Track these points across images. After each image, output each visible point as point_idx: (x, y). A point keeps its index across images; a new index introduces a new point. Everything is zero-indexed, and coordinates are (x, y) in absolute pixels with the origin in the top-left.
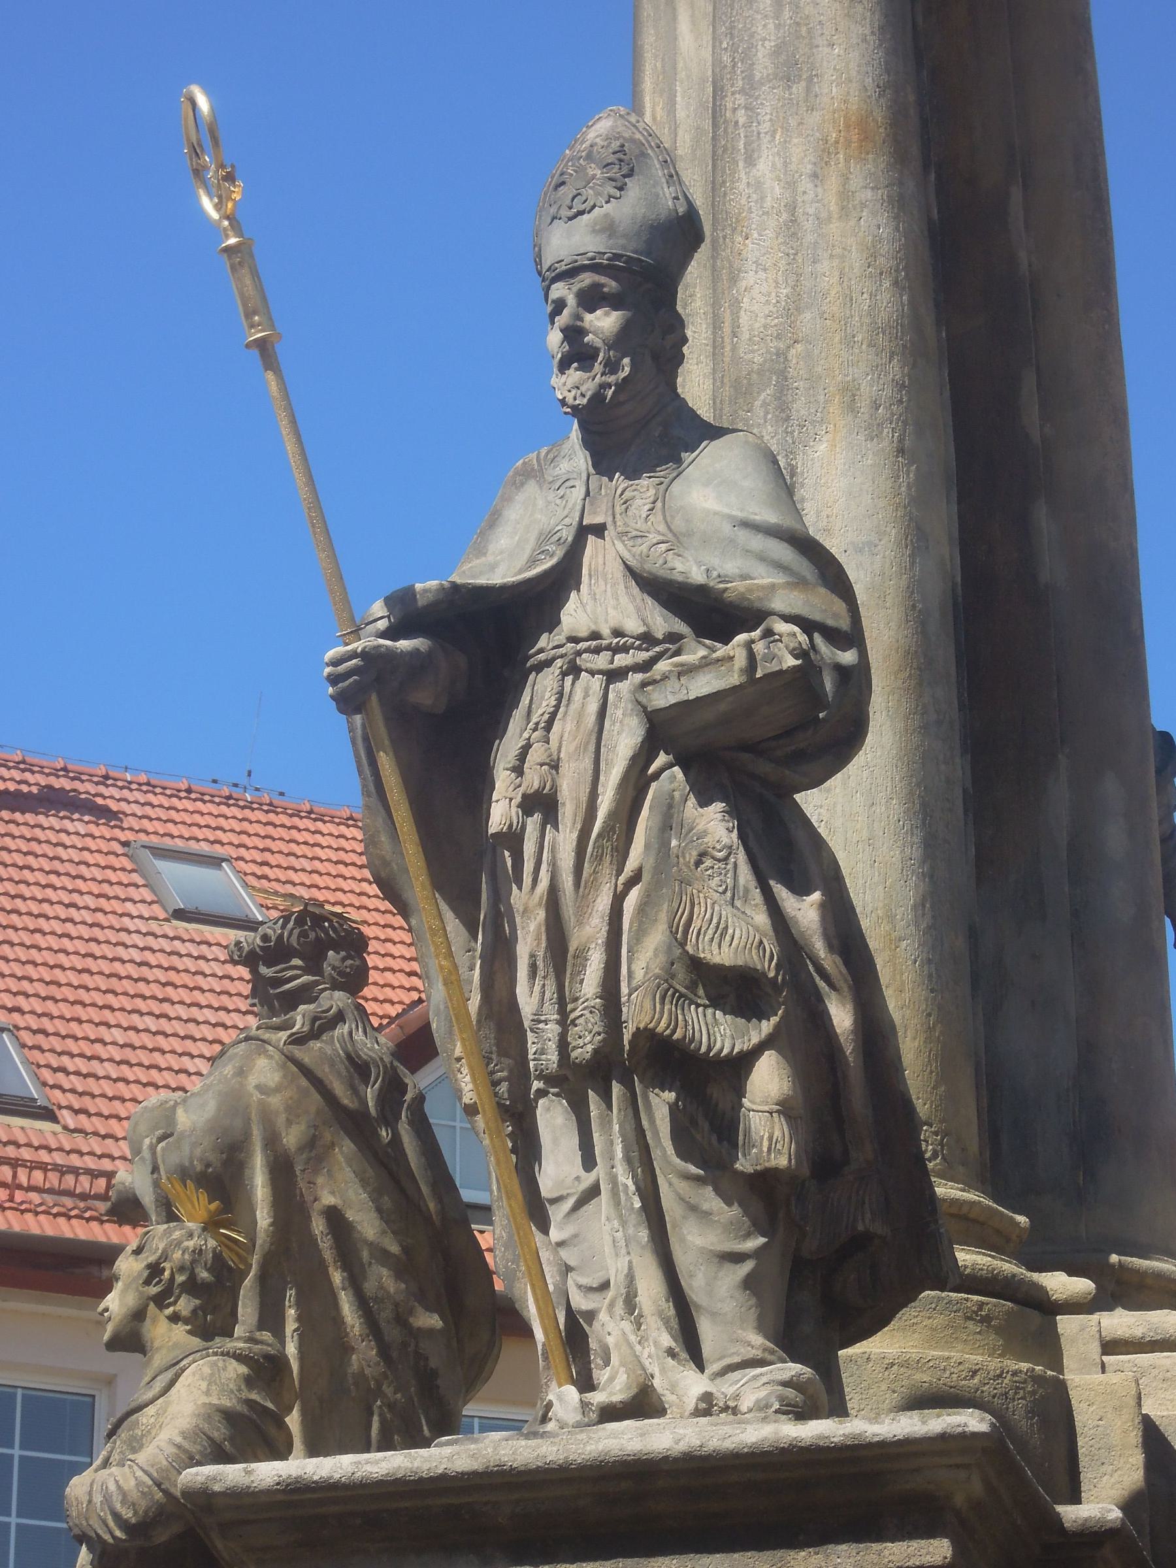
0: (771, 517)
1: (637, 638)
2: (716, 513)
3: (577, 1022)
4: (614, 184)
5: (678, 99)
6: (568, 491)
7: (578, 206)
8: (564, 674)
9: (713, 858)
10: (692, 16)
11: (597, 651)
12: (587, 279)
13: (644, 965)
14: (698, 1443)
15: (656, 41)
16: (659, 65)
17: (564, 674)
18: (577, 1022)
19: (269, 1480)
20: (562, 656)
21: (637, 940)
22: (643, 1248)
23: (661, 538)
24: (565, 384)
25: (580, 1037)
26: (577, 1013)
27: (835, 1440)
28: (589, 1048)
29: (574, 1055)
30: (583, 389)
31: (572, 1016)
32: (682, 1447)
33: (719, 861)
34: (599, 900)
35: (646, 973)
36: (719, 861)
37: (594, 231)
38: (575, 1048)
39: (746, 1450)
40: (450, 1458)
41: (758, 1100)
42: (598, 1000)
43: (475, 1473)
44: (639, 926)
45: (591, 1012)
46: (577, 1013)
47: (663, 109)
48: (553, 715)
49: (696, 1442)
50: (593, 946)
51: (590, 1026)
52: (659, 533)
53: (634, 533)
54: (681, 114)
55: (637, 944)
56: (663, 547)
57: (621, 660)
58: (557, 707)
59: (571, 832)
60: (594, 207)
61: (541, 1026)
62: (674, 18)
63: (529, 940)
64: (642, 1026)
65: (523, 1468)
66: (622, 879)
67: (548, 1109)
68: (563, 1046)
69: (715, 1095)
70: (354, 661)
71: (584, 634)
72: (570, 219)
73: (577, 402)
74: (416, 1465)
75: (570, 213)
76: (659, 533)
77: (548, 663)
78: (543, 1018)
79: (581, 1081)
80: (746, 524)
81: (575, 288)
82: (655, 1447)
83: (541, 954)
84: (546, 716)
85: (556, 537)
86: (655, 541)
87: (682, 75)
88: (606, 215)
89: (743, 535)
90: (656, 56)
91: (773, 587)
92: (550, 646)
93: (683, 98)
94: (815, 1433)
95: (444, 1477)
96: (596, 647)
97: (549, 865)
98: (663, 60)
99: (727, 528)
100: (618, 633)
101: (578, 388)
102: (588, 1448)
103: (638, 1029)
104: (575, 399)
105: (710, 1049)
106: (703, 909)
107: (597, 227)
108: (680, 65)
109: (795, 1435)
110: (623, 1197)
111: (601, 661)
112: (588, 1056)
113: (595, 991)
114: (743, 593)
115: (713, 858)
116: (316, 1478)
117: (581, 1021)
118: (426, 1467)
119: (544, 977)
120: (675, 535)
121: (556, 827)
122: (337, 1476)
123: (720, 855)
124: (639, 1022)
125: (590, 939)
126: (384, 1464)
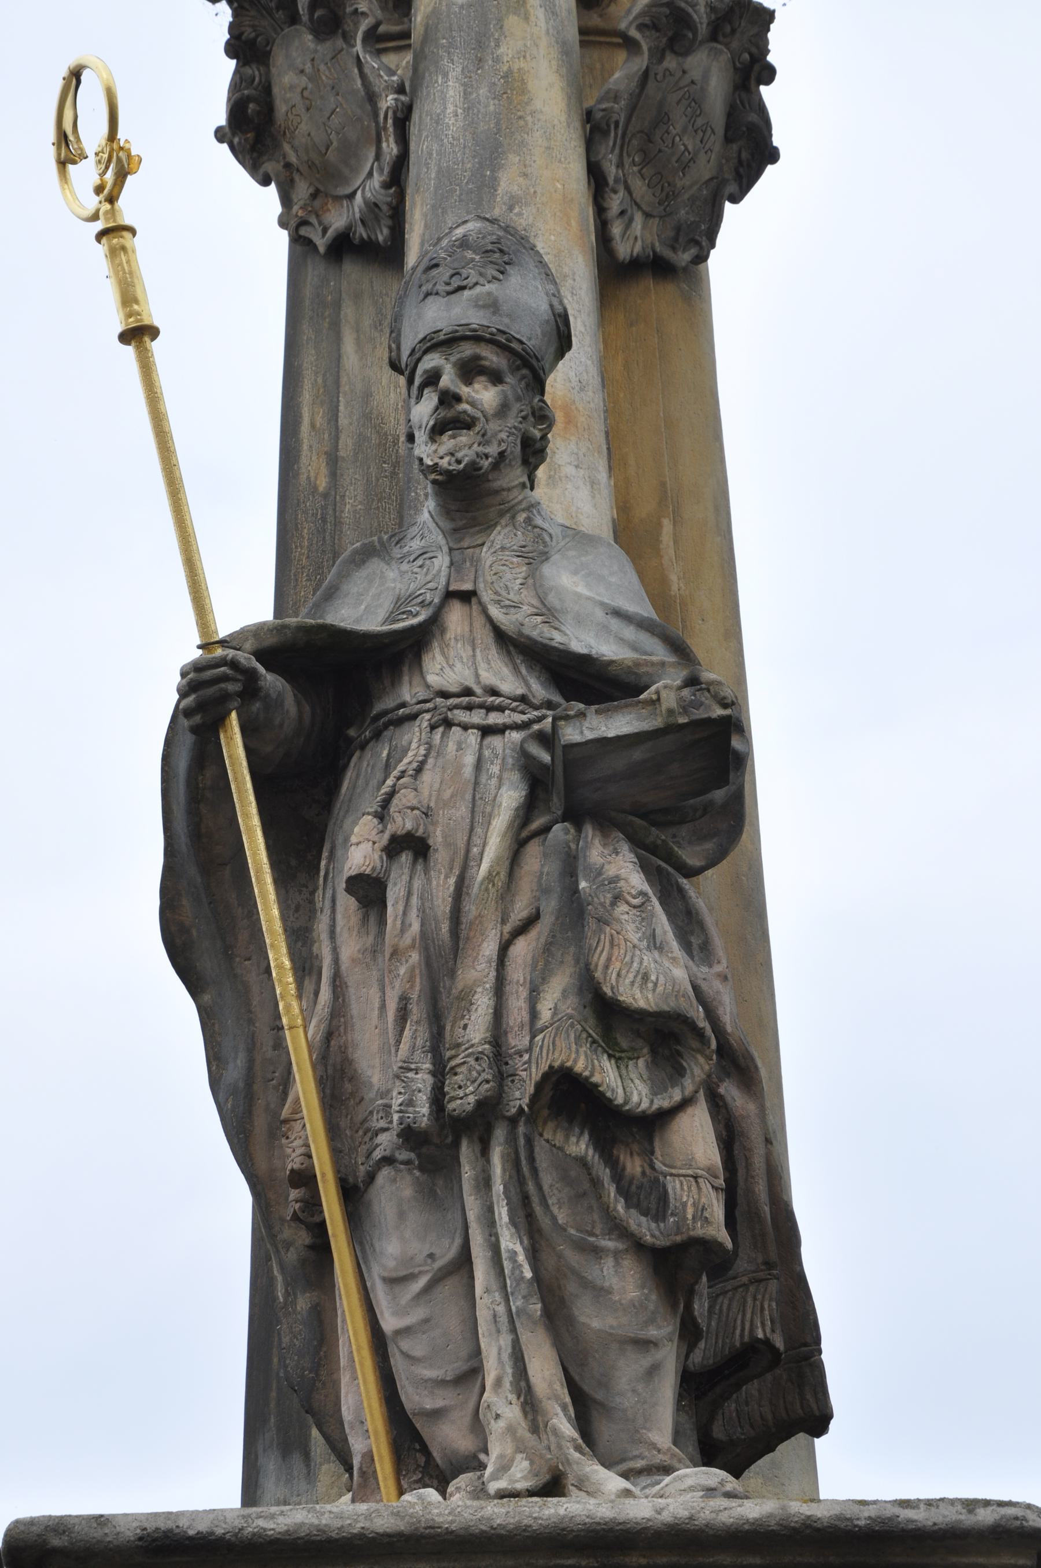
0: (645, 610)
1: (514, 699)
2: (589, 598)
3: (459, 1070)
4: (497, 267)
5: (341, 408)
6: (428, 562)
7: (456, 282)
8: (433, 727)
9: (627, 903)
10: (358, 339)
11: (469, 708)
12: (467, 350)
13: (552, 1006)
14: (686, 1514)
15: (317, 359)
16: (320, 380)
17: (433, 727)
18: (459, 1070)
19: (129, 1533)
20: (428, 711)
21: (543, 979)
22: (535, 1323)
23: (535, 610)
24: (435, 451)
25: (460, 1087)
26: (458, 1061)
27: (859, 1523)
28: (472, 1099)
29: (451, 1106)
30: (459, 455)
31: (453, 1063)
32: (666, 1517)
33: (635, 907)
34: (485, 945)
35: (555, 1014)
36: (635, 907)
37: (477, 306)
38: (454, 1099)
39: (747, 1527)
40: (368, 1517)
41: (679, 1164)
42: (487, 1046)
43: (400, 1535)
44: (545, 965)
45: (477, 1059)
46: (458, 1061)
47: (322, 418)
48: (423, 763)
49: (684, 1514)
50: (479, 990)
51: (474, 1074)
52: (533, 606)
53: (507, 603)
54: (343, 421)
55: (543, 984)
56: (539, 619)
57: (495, 719)
58: (426, 756)
59: (447, 877)
60: (476, 284)
61: (410, 1075)
62: (338, 339)
63: (397, 984)
64: (556, 1064)
65: (462, 1532)
66: (508, 928)
67: (394, 1180)
68: (438, 1098)
69: (622, 1158)
70: (222, 669)
71: (454, 689)
72: (449, 293)
73: (451, 468)
74: (324, 1522)
75: (449, 288)
76: (533, 606)
77: (414, 717)
78: (413, 1066)
79: (437, 1147)
80: (617, 613)
81: (453, 359)
82: (631, 1515)
83: (414, 996)
84: (415, 765)
85: (420, 599)
86: (529, 612)
87: (345, 388)
88: (489, 294)
89: (615, 623)
90: (316, 373)
91: (663, 664)
92: (414, 701)
93: (346, 408)
94: (832, 1513)
95: (361, 1536)
96: (469, 703)
97: (419, 910)
98: (324, 375)
99: (599, 614)
100: (494, 692)
101: (452, 454)
102: (547, 1512)
103: (551, 1067)
104: (450, 464)
105: (626, 1102)
106: (622, 951)
107: (481, 303)
108: (344, 380)
109: (809, 1513)
110: (507, 1265)
111: (477, 717)
112: (469, 1108)
113: (483, 1036)
114: (629, 667)
115: (627, 903)
116: (191, 1533)
117: (463, 1069)
118: (338, 1523)
119: (418, 1022)
120: (549, 610)
121: (426, 871)
122: (219, 1531)
123: (636, 902)
124: (553, 1060)
125: (478, 982)
126: (281, 1519)
